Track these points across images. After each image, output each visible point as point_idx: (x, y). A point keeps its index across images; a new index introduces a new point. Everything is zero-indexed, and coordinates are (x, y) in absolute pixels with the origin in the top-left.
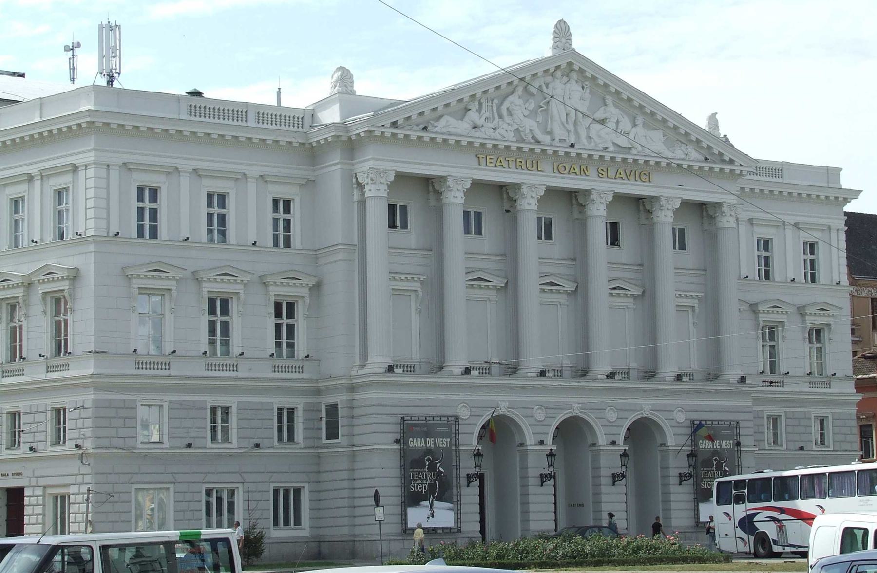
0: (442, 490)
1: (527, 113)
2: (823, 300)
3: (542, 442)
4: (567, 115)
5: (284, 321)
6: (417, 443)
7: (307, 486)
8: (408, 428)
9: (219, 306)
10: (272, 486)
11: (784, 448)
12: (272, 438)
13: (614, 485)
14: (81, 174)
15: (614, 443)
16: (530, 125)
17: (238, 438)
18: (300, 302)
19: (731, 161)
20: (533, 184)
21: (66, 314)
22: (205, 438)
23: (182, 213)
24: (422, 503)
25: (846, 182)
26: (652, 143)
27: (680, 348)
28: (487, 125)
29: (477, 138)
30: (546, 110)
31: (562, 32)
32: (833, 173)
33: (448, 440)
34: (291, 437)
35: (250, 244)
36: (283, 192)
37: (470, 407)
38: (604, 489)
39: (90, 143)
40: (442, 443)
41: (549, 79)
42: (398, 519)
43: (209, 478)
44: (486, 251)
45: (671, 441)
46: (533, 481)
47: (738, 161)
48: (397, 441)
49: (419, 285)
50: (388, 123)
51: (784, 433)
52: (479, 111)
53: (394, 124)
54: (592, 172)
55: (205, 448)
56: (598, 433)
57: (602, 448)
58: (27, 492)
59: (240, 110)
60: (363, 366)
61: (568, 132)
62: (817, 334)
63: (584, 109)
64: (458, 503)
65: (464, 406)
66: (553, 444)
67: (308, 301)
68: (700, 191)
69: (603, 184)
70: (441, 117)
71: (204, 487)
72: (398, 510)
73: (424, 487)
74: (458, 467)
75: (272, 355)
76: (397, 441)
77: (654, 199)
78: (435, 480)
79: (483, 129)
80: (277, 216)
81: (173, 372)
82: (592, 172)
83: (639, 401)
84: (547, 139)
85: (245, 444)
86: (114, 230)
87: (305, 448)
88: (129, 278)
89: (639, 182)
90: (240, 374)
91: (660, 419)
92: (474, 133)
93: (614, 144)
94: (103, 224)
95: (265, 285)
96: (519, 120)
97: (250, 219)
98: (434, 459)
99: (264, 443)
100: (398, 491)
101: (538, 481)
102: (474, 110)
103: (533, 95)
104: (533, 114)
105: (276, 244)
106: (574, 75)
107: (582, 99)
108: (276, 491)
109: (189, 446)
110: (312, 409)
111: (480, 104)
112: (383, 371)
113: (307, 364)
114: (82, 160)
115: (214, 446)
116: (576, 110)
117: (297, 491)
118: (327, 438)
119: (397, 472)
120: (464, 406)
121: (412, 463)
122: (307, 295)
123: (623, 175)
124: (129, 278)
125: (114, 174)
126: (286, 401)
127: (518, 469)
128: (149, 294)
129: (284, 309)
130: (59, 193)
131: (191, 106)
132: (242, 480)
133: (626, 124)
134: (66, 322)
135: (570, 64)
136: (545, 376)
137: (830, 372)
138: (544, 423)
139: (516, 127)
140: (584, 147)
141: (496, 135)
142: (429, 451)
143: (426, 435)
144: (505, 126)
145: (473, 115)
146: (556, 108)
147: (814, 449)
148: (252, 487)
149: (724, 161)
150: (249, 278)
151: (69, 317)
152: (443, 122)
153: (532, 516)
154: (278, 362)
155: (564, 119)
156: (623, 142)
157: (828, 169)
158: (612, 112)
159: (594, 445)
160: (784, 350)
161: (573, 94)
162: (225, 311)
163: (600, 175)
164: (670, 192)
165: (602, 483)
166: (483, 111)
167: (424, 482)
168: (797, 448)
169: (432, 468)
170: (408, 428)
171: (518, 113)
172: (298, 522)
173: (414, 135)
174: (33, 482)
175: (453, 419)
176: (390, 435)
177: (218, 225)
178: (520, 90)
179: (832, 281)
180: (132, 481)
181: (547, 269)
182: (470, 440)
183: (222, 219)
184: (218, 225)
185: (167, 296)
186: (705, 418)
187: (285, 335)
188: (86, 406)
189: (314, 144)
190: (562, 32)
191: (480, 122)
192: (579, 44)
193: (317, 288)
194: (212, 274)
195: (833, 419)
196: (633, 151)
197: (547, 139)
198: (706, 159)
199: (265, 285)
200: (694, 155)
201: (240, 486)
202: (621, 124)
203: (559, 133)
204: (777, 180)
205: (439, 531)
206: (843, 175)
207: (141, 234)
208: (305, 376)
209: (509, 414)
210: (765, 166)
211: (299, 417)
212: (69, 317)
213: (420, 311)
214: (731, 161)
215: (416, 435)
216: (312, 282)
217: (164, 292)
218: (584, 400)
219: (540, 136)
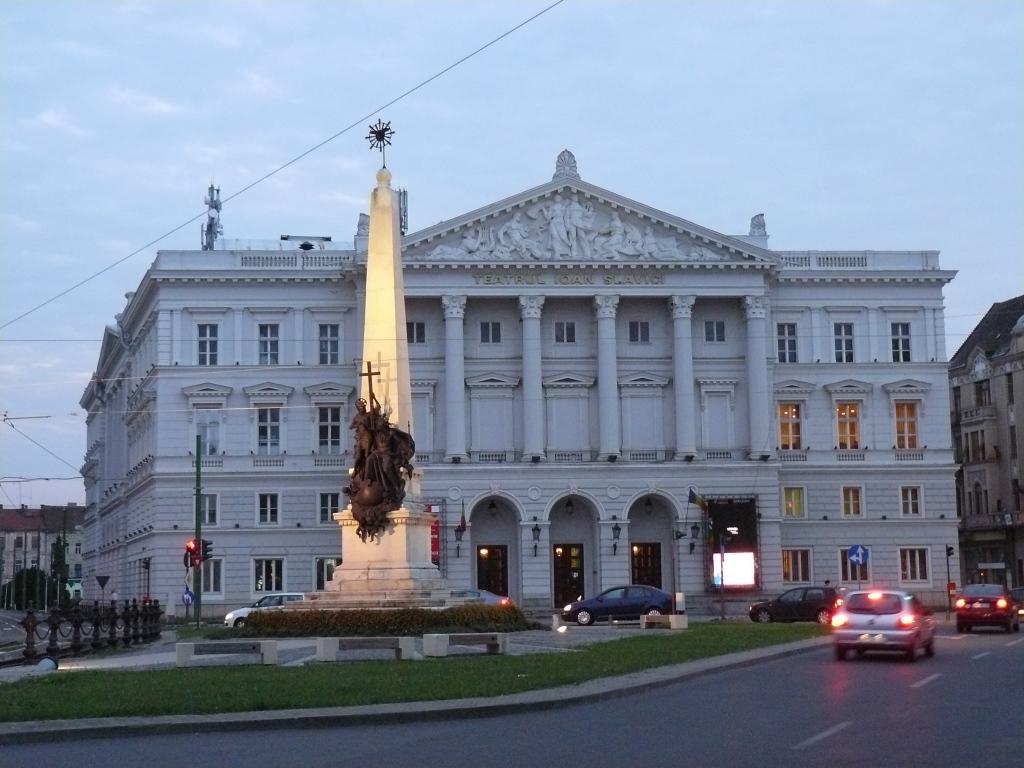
4: (568, 233)
5: (329, 423)
11: (806, 517)
19: (751, 258)
25: (944, 264)
26: (671, 251)
28: (483, 248)
29: (469, 261)
30: (547, 230)
36: (328, 319)
43: (317, 550)
44: (428, 356)
51: (864, 503)
63: (589, 226)
69: (611, 290)
79: (477, 253)
83: (646, 480)
85: (289, 524)
90: (285, 469)
93: (619, 253)
95: (829, 393)
104: (531, 234)
107: (584, 217)
124: (187, 397)
138: (619, 500)
139: (512, 248)
148: (295, 558)
155: (564, 236)
156: (630, 251)
162: (275, 418)
168: (821, 517)
171: (516, 236)
172: (924, 575)
173: (734, 265)
177: (846, 353)
184: (846, 353)
190: (566, 160)
195: (867, 489)
196: (641, 258)
199: (829, 393)
200: (709, 255)
203: (559, 249)
204: (290, 268)
207: (896, 357)
209: (580, 494)
210: (849, 256)
214: (751, 258)
216: (348, 392)
217: (854, 404)
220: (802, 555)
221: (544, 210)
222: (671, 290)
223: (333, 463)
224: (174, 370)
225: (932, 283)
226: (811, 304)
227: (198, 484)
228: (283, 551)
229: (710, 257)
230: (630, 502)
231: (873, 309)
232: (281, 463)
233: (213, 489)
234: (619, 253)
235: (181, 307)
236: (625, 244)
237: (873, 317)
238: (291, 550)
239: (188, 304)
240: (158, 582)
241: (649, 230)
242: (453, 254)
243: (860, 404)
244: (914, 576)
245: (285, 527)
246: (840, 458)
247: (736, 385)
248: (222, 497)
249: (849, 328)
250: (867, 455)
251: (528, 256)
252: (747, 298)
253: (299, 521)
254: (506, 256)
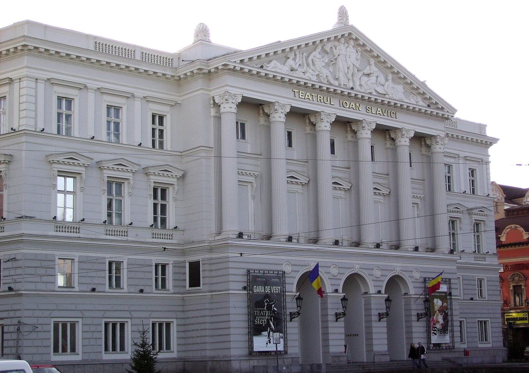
0: (278, 324)
1: (324, 64)
2: (481, 205)
3: (336, 291)
4: (348, 68)
6: (259, 289)
7: (175, 320)
8: (253, 279)
9: (115, 186)
10: (151, 320)
12: (152, 286)
13: (337, 321)
14: (16, 85)
15: (379, 292)
16: (325, 72)
17: (128, 285)
18: (171, 188)
19: (442, 108)
20: (329, 111)
22: (105, 284)
23: (89, 119)
24: (263, 333)
25: (490, 133)
26: (396, 93)
27: (413, 232)
28: (299, 69)
31: (343, 13)
32: (482, 127)
33: (279, 288)
34: (164, 286)
35: (137, 144)
37: (293, 266)
38: (330, 324)
39: (26, 60)
40: (276, 290)
41: (336, 43)
42: (246, 345)
43: (107, 314)
45: (412, 291)
46: (331, 318)
47: (446, 109)
48: (245, 288)
49: (254, 178)
52: (294, 59)
53: (242, 61)
54: (362, 108)
55: (104, 292)
57: (372, 295)
59: (130, 49)
60: (219, 234)
61: (349, 80)
64: (285, 333)
65: (287, 264)
66: (343, 292)
67: (176, 188)
70: (271, 61)
72: (246, 338)
73: (264, 322)
74: (285, 308)
75: (105, 222)
76: (245, 288)
78: (271, 317)
79: (297, 72)
80: (154, 127)
84: (336, 83)
85: (85, 288)
86: (40, 127)
89: (390, 118)
91: (405, 276)
92: (291, 73)
93: (375, 90)
96: (315, 71)
97: (136, 127)
98: (270, 302)
99: (146, 289)
100: (246, 324)
101: (377, 318)
102: (291, 58)
103: (328, 53)
105: (154, 146)
109: (94, 290)
110: (178, 265)
111: (295, 55)
112: (235, 236)
113: (175, 233)
114: (15, 76)
115: (112, 291)
116: (354, 65)
117: (168, 325)
118: (190, 286)
119: (246, 311)
120: (287, 264)
121: (257, 304)
122: (176, 184)
123: (381, 112)
124: (51, 163)
125: (41, 86)
126: (161, 259)
127: (320, 310)
128: (64, 176)
129: (160, 193)
131: (96, 43)
132: (81, 316)
133: (382, 79)
135: (350, 34)
136: (338, 244)
137: (485, 251)
139: (317, 73)
140: (359, 91)
141: (305, 77)
142: (266, 296)
143: (265, 284)
144: (311, 71)
145: (290, 62)
146: (341, 63)
147: (478, 299)
148: (138, 321)
150: (137, 168)
152: (272, 64)
153: (331, 343)
154: (110, 228)
156: (380, 90)
157: (480, 125)
158: (373, 69)
159: (366, 293)
161: (348, 55)
164: (408, 125)
165: (373, 320)
166: (297, 60)
167: (264, 317)
168: (469, 299)
169: (269, 308)
170: (253, 279)
171: (319, 64)
175: (281, 273)
176: (241, 283)
178: (319, 49)
179: (484, 194)
180: (51, 316)
181: (336, 174)
182: (292, 289)
183: (117, 125)
186: (428, 276)
187: (160, 212)
188: (17, 258)
190: (343, 13)
191: (296, 67)
192: (352, 22)
194: (111, 164)
195: (463, 280)
196: (387, 96)
197: (336, 83)
198: (429, 106)
201: (129, 320)
202: (379, 78)
205: (272, 353)
206: (487, 129)
208: (174, 241)
211: (170, 270)
213: (254, 198)
215: (258, 284)
216: (180, 174)
218: (362, 262)
219: (332, 81)
220: (71, 325)
221: (334, 48)
222: (438, 132)
223: (165, 236)
229: (422, 104)
230: (344, 278)
232: (171, 237)
233: (72, 253)
234: (375, 90)
235: (46, 77)
236: (371, 84)
240: (26, 343)
241: (390, 77)
242: (276, 67)
243: (126, 182)
246: (154, 236)
247: (256, 177)
250: (82, 227)
254: (314, 78)
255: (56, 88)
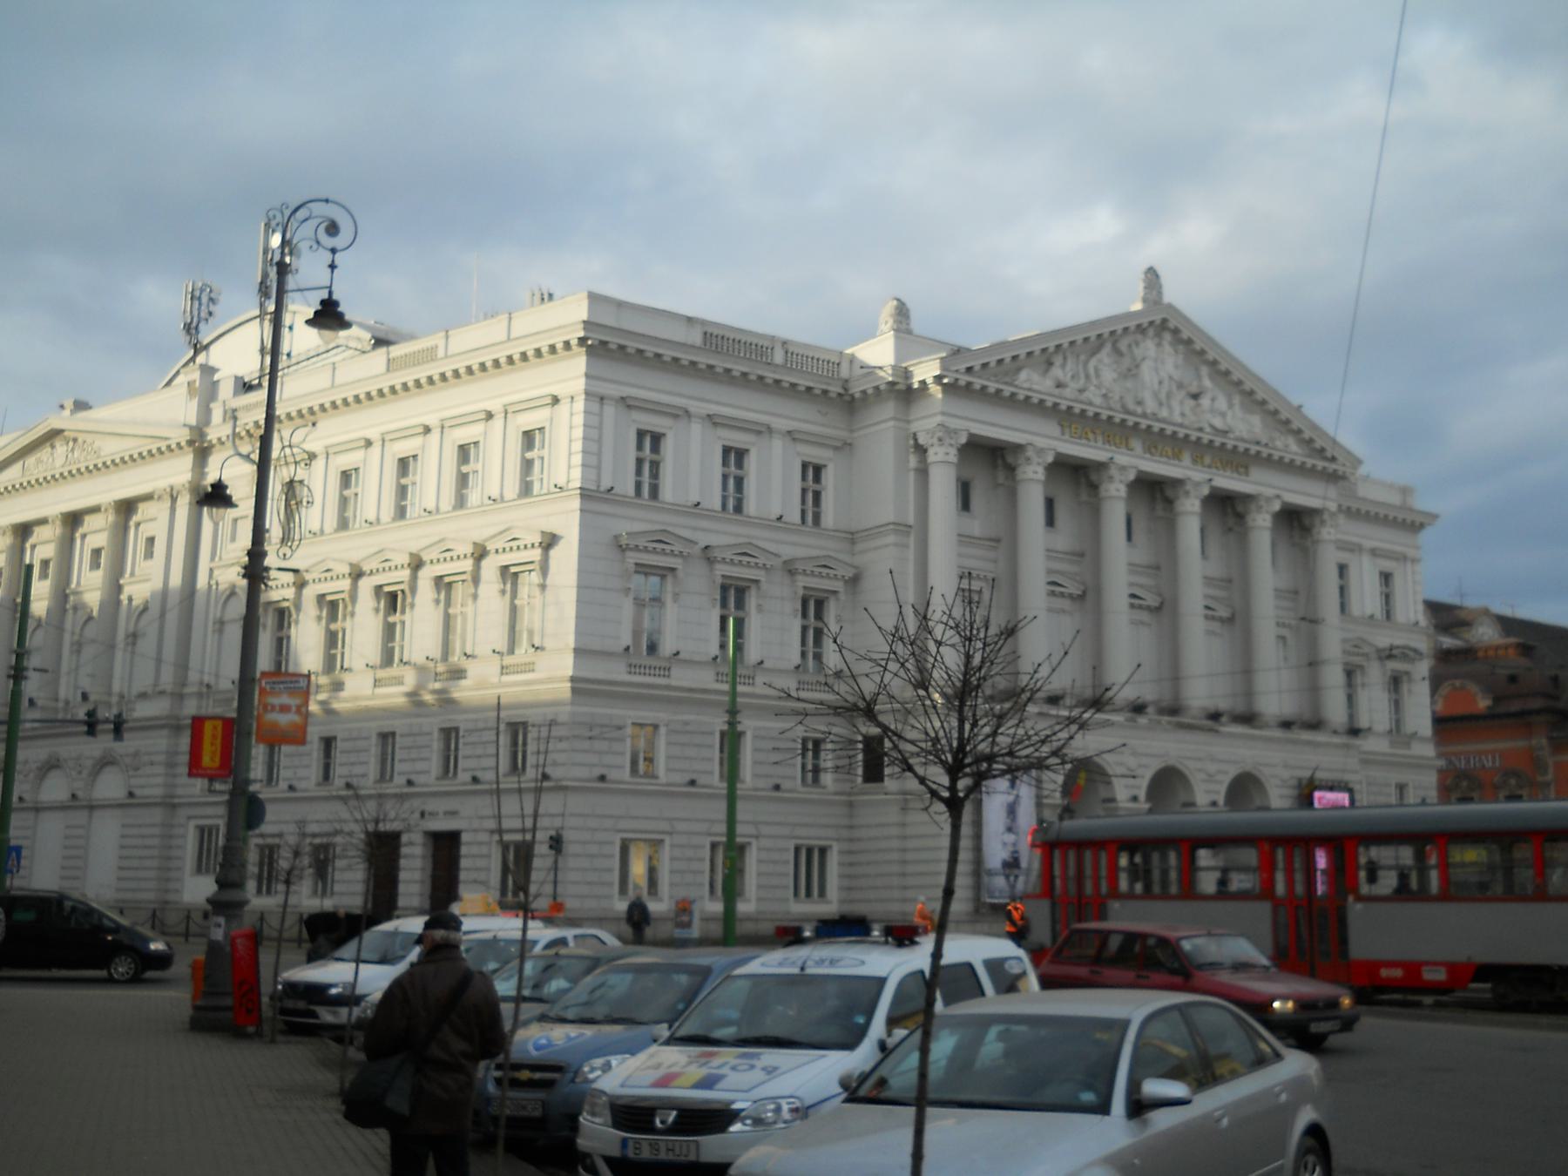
9: (734, 594)
21: (403, 612)
23: (692, 468)
31: (1152, 278)
36: (815, 454)
41: (1139, 337)
43: (623, 824)
47: (1341, 459)
50: (963, 367)
52: (1063, 366)
53: (969, 370)
54: (1187, 458)
56: (1196, 788)
58: (465, 837)
62: (1396, 682)
68: (1305, 494)
71: (791, 845)
77: (1248, 498)
81: (674, 682)
82: (1187, 458)
85: (761, 783)
86: (605, 484)
87: (836, 794)
88: (622, 549)
94: (594, 477)
95: (711, 561)
96: (1099, 386)
99: (786, 784)
106: (1167, 336)
108: (797, 849)
117: (823, 851)
124: (622, 549)
130: (404, 465)
133: (1222, 403)
134: (403, 623)
135: (1164, 321)
145: (1057, 372)
149: (1326, 459)
151: (348, 624)
156: (1218, 423)
160: (1363, 697)
163: (1195, 461)
174: (476, 824)
185: (670, 579)
189: (857, 395)
192: (1170, 295)
193: (854, 581)
200: (1294, 447)
201: (754, 841)
212: (407, 617)
214: (1333, 459)
216: (849, 573)
217: (665, 572)
224: (606, 500)
225: (734, 377)
226: (693, 406)
227: (733, 712)
228: (664, 826)
229: (1292, 449)
231: (611, 398)
232: (666, 671)
237: (696, 428)
238: (765, 830)
239: (714, 409)
241: (1237, 400)
244: (809, 894)
245: (756, 789)
248: (755, 737)
249: (657, 439)
251: (1118, 407)
252: (1030, 448)
253: (778, 781)
254: (1098, 401)
255: (636, 415)
